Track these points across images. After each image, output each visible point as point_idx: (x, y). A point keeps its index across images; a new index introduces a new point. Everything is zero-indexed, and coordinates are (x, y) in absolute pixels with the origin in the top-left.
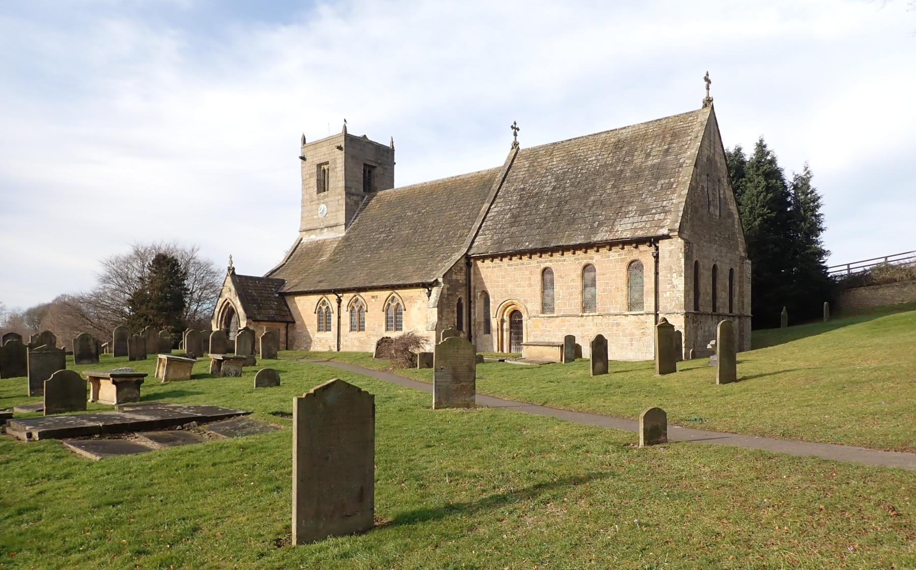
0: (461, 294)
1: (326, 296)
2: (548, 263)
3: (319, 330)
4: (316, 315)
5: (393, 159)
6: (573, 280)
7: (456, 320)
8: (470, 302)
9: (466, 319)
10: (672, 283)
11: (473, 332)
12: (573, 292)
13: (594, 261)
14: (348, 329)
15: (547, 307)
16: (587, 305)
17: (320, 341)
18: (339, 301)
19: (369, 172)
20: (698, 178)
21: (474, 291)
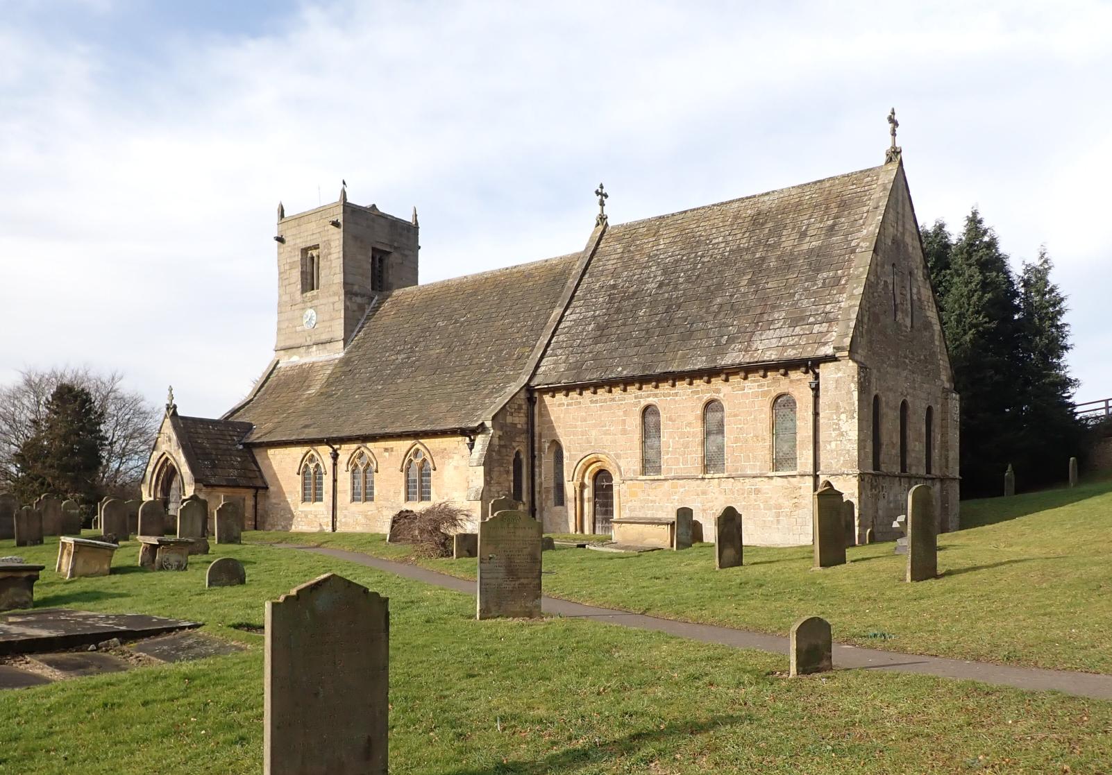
0: (520, 446)
3: (304, 500)
4: (300, 478)
6: (689, 425)
7: (512, 484)
8: (533, 457)
11: (537, 503)
13: (721, 395)
14: (349, 498)
15: (649, 464)
16: (711, 463)
17: (306, 516)
18: (335, 456)
19: (381, 260)
21: (540, 441)
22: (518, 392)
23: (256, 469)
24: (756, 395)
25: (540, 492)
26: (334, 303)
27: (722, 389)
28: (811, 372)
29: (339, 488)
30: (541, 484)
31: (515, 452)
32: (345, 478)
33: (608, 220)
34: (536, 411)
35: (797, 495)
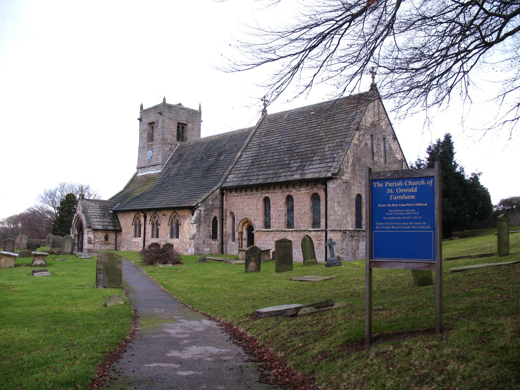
0: (216, 213)
1: (176, 211)
2: (266, 194)
3: (135, 236)
4: (133, 227)
5: (200, 118)
6: (281, 206)
7: (211, 232)
8: (223, 219)
9: (220, 231)
10: (335, 209)
11: (224, 240)
12: (280, 214)
13: (292, 193)
14: (150, 236)
15: (267, 225)
16: (290, 224)
17: (135, 244)
18: (145, 217)
19: (183, 128)
20: (361, 137)
21: (226, 212)
22: (216, 190)
23: (117, 222)
24: (305, 194)
25: (225, 235)
26: (159, 147)
27: (294, 192)
28: (34, 264)
29: (146, 240)
30: (226, 232)
31: (213, 217)
32: (149, 227)
33: (267, 112)
34: (224, 198)
35: (320, 239)
